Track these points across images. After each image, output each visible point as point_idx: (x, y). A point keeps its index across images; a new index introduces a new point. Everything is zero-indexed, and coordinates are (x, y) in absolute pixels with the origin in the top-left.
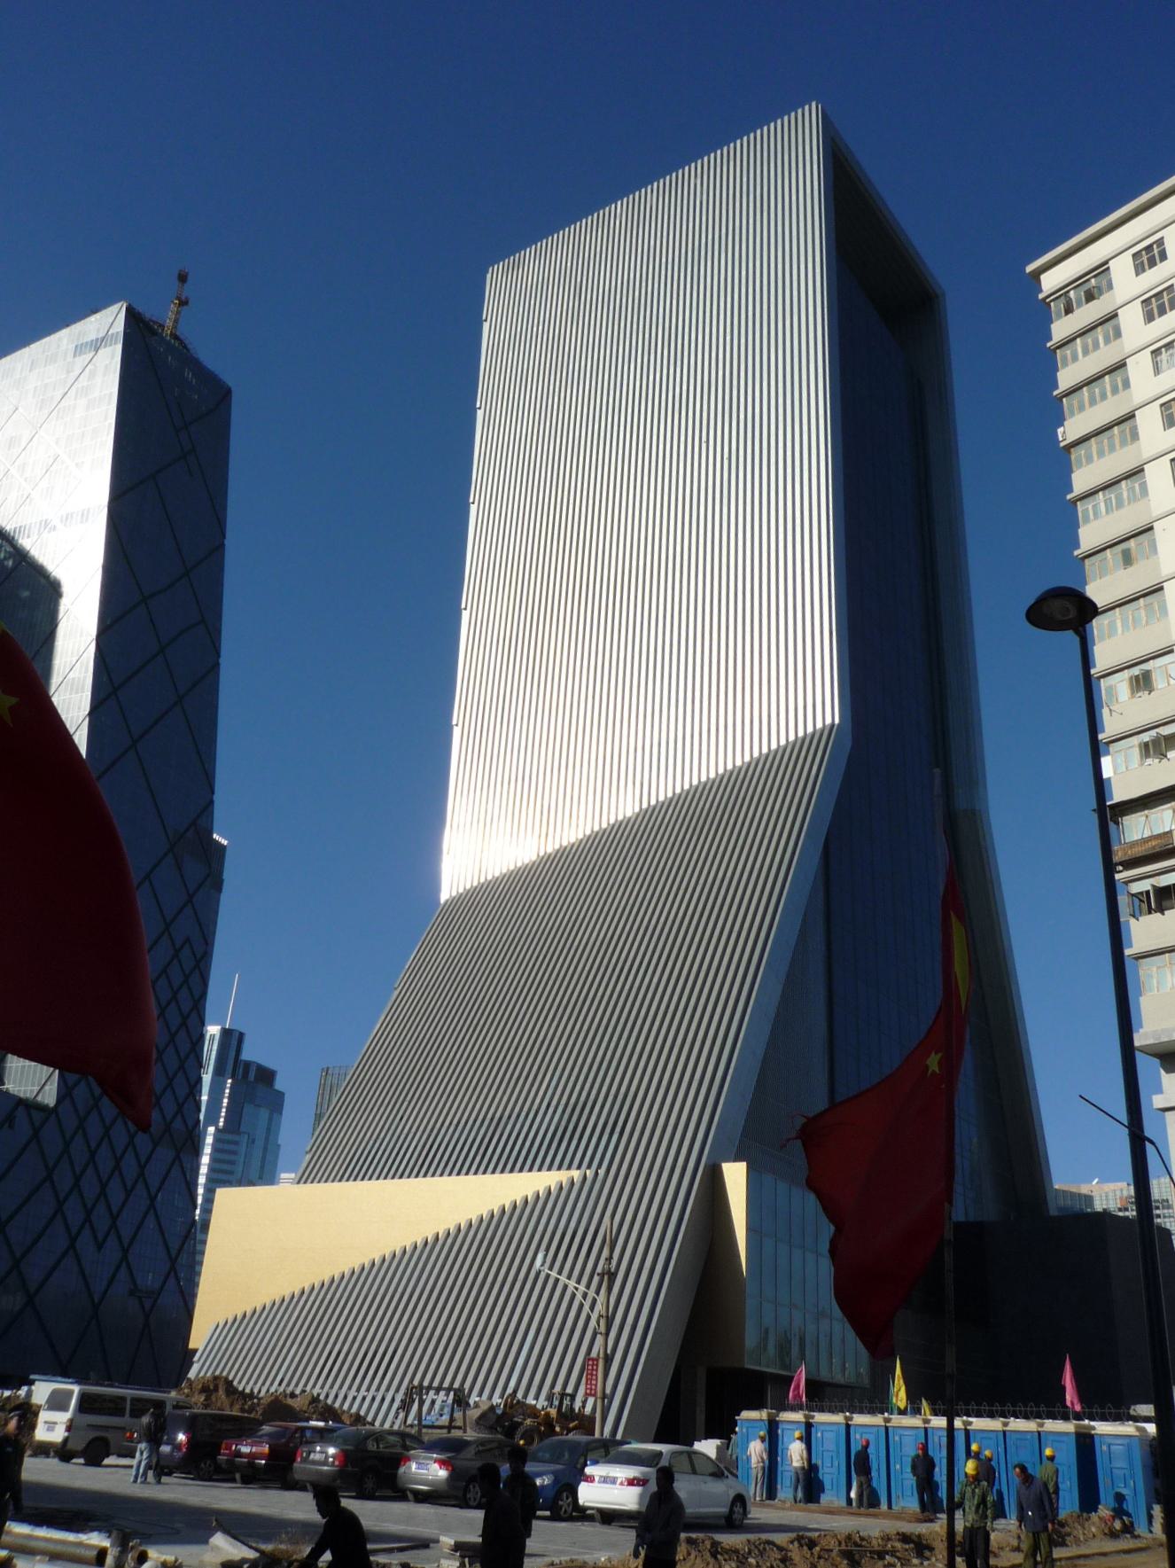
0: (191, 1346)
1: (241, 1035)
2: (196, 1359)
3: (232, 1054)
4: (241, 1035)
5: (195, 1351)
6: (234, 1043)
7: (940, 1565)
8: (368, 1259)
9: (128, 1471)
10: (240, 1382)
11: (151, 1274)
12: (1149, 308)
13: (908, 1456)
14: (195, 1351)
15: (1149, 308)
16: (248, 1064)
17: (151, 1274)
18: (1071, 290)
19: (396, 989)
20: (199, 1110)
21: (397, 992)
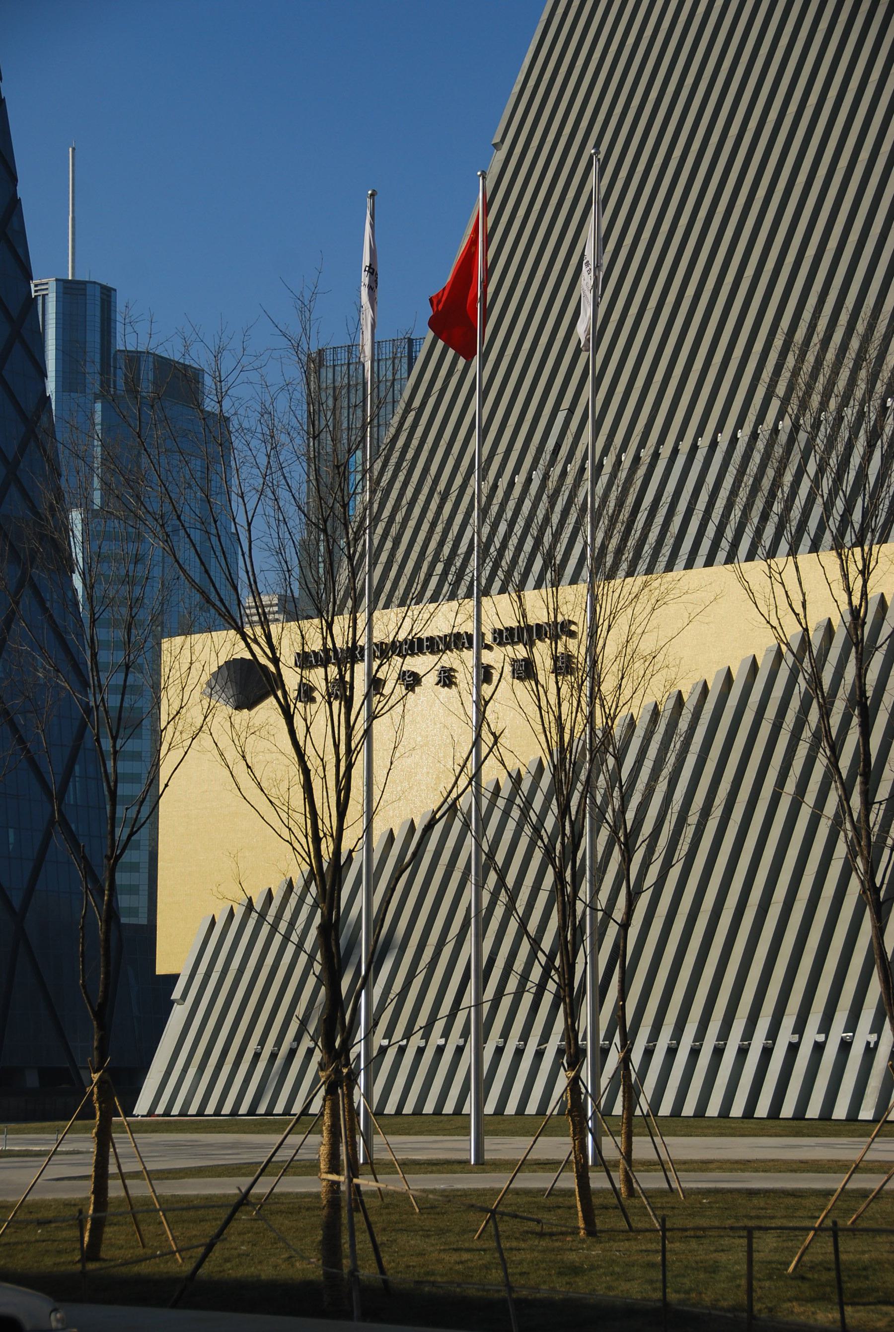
0: (161, 969)
1: (107, 293)
2: (176, 994)
3: (94, 339)
4: (107, 293)
5: (175, 978)
6: (94, 312)
7: (2, 1263)
8: (715, 670)
9: (90, 1155)
10: (310, 1052)
11: (11, 832)
12: (98, 1215)
13: (657, 1281)
14: (175, 978)
15: (98, 1215)
16: (134, 358)
17: (11, 832)
18: (158, 1116)
19: (497, 146)
20: (44, 374)
21: (501, 155)
